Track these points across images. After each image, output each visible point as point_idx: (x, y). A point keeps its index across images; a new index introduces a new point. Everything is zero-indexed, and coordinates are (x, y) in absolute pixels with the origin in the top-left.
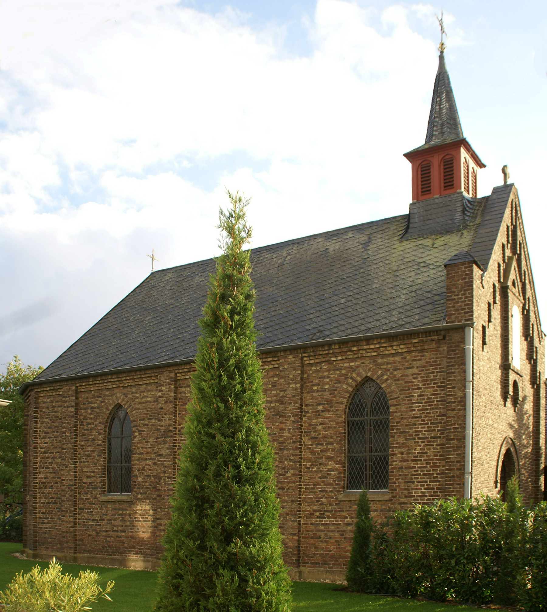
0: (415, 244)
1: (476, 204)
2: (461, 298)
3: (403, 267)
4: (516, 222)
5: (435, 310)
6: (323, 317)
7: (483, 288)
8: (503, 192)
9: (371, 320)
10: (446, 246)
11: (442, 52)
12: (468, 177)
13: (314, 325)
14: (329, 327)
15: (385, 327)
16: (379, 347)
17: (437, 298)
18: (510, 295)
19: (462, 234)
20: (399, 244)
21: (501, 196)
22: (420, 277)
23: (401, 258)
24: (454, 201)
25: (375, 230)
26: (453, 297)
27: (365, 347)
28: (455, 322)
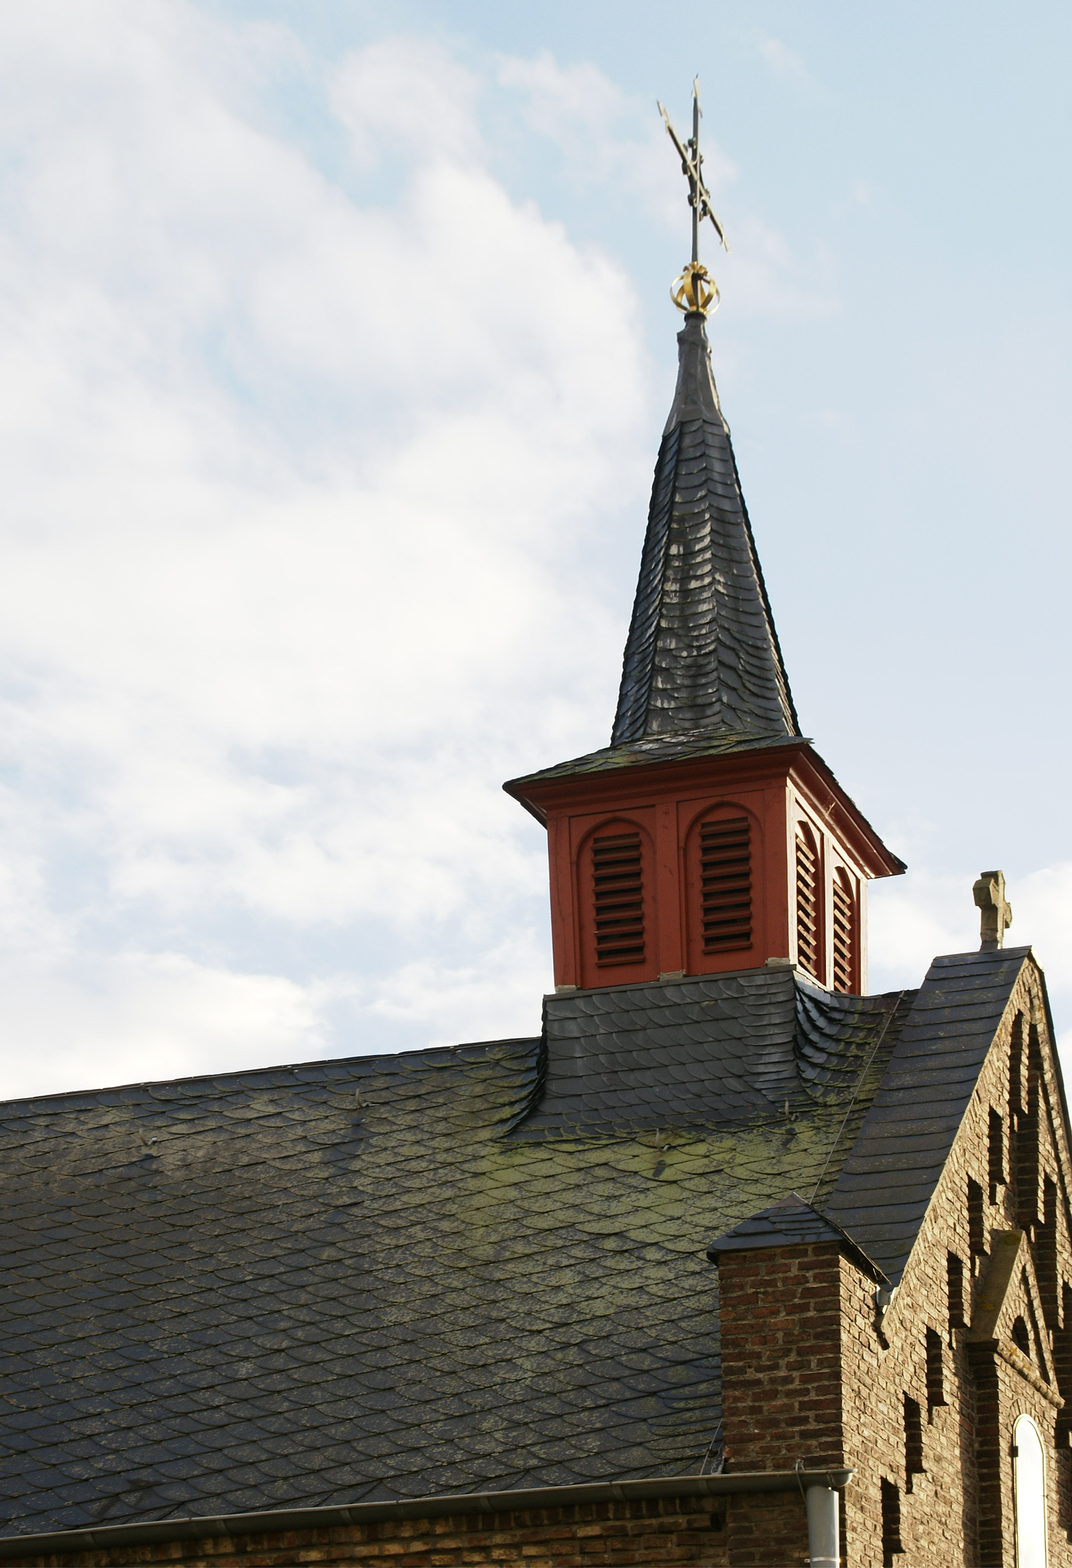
0: (573, 1162)
1: (854, 1020)
2: (788, 1380)
3: (520, 1248)
4: (1033, 1105)
5: (671, 1420)
6: (153, 1431)
7: (885, 1345)
8: (978, 982)
9: (385, 1447)
10: (716, 1178)
11: (695, 318)
12: (819, 906)
13: (110, 1462)
14: (183, 1470)
15: (447, 1477)
16: (428, 1552)
17: (678, 1374)
18: (1004, 1373)
19: (792, 1134)
20: (500, 1159)
21: (966, 998)
22: (604, 1291)
23: (510, 1213)
24: (751, 1001)
25: (385, 1096)
26: (751, 1374)
27: (363, 1551)
28: (764, 1468)
